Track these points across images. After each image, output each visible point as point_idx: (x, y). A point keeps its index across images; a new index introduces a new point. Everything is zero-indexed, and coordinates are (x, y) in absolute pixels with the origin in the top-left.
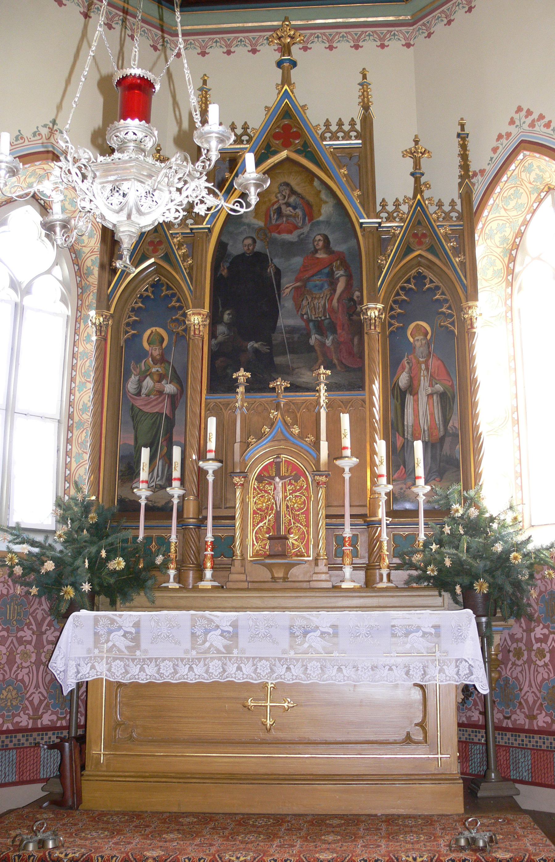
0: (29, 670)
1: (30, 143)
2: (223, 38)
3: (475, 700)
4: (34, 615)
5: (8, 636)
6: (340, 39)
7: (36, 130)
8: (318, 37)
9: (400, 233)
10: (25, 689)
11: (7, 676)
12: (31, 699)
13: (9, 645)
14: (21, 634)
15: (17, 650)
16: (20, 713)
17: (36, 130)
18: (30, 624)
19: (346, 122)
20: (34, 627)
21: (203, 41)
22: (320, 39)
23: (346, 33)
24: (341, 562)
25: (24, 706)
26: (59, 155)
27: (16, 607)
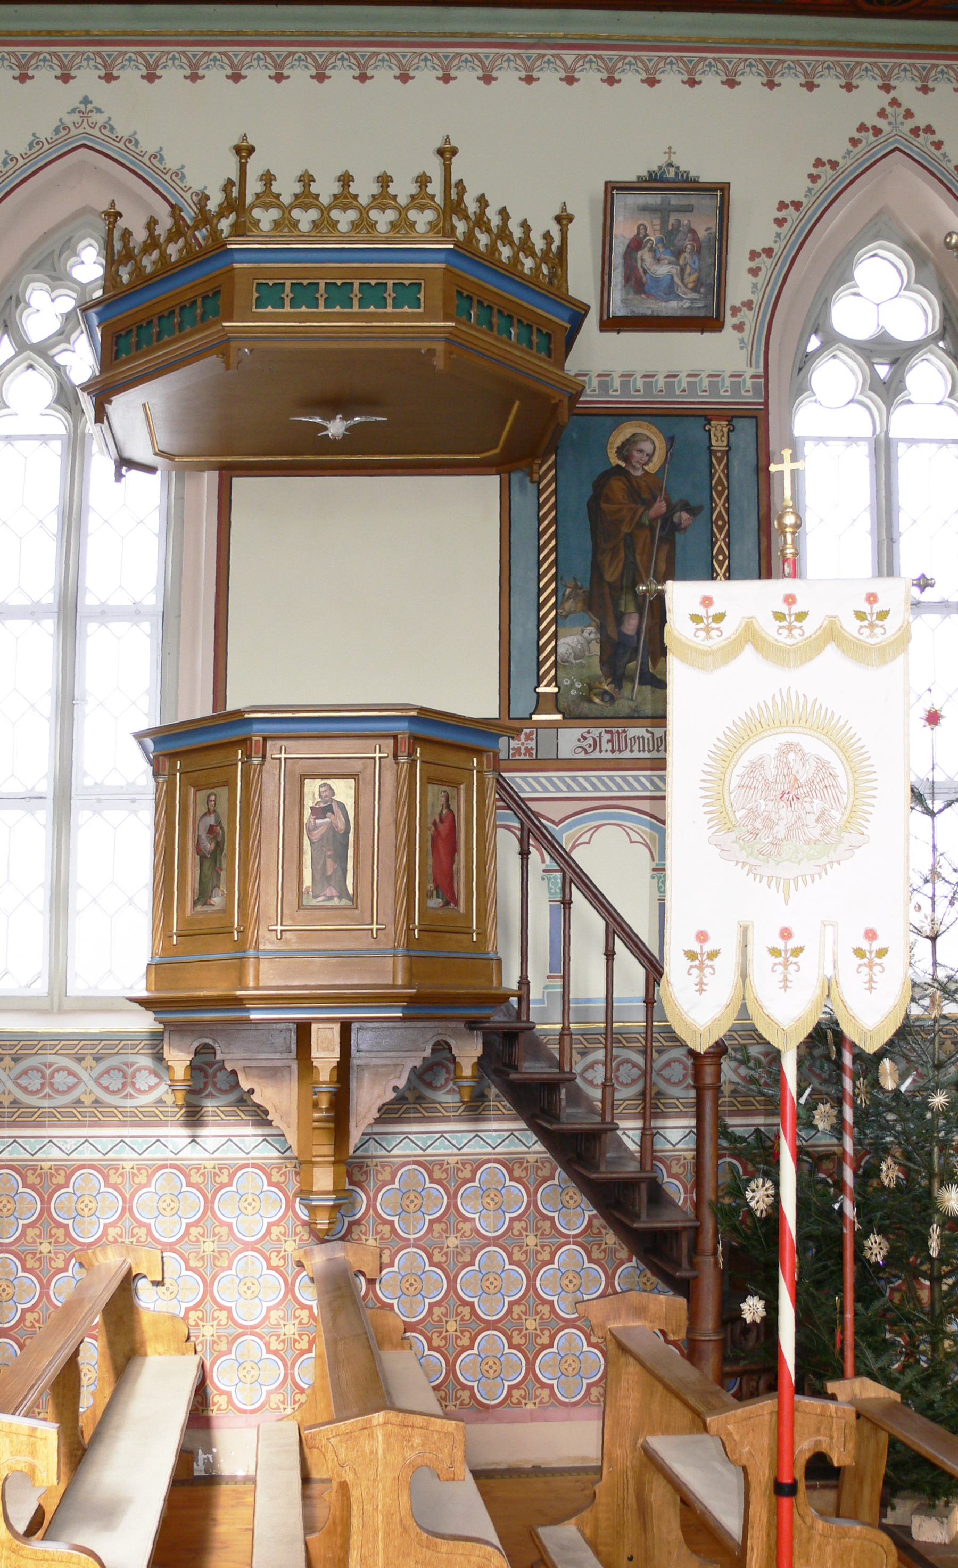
1: (170, 181)
2: (760, 59)
6: (294, 63)
7: (5, 156)
8: (174, 58)
9: (744, 397)
17: (5, 156)
19: (326, 189)
21: (610, 59)
22: (177, 62)
23: (388, 54)
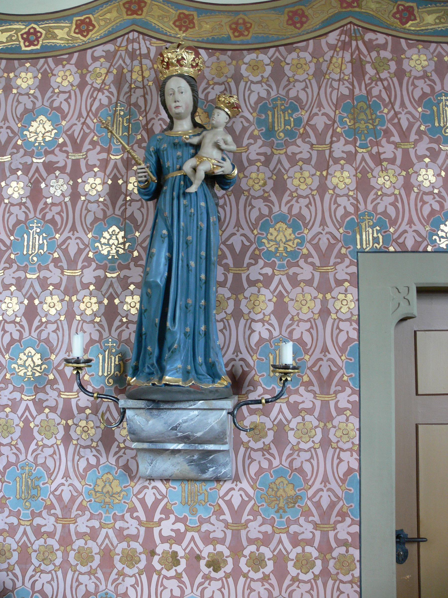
0: (55, 451)
3: (295, 129)
4: (64, 247)
5: (19, 524)
10: (49, 478)
11: (22, 457)
12: (57, 493)
13: (21, 538)
14: (38, 521)
15: (32, 544)
16: (54, 150)
18: (52, 507)
20: (58, 511)
24: (287, 168)
25: (49, 503)
26: (203, 308)
27: (37, 237)
